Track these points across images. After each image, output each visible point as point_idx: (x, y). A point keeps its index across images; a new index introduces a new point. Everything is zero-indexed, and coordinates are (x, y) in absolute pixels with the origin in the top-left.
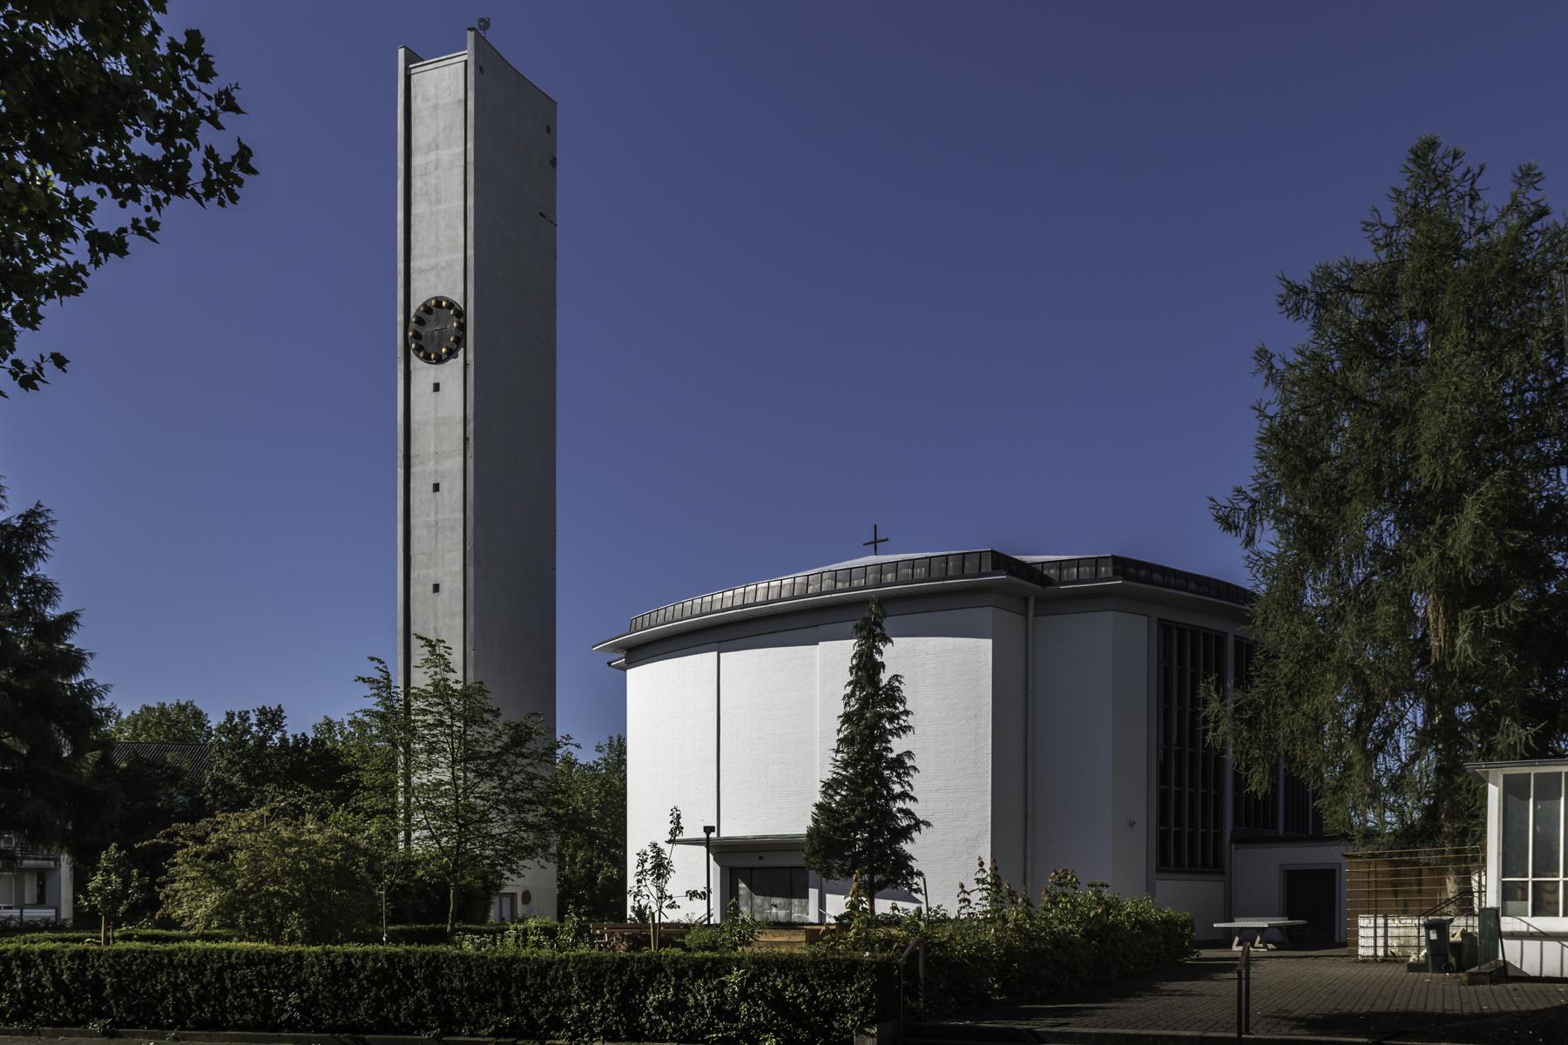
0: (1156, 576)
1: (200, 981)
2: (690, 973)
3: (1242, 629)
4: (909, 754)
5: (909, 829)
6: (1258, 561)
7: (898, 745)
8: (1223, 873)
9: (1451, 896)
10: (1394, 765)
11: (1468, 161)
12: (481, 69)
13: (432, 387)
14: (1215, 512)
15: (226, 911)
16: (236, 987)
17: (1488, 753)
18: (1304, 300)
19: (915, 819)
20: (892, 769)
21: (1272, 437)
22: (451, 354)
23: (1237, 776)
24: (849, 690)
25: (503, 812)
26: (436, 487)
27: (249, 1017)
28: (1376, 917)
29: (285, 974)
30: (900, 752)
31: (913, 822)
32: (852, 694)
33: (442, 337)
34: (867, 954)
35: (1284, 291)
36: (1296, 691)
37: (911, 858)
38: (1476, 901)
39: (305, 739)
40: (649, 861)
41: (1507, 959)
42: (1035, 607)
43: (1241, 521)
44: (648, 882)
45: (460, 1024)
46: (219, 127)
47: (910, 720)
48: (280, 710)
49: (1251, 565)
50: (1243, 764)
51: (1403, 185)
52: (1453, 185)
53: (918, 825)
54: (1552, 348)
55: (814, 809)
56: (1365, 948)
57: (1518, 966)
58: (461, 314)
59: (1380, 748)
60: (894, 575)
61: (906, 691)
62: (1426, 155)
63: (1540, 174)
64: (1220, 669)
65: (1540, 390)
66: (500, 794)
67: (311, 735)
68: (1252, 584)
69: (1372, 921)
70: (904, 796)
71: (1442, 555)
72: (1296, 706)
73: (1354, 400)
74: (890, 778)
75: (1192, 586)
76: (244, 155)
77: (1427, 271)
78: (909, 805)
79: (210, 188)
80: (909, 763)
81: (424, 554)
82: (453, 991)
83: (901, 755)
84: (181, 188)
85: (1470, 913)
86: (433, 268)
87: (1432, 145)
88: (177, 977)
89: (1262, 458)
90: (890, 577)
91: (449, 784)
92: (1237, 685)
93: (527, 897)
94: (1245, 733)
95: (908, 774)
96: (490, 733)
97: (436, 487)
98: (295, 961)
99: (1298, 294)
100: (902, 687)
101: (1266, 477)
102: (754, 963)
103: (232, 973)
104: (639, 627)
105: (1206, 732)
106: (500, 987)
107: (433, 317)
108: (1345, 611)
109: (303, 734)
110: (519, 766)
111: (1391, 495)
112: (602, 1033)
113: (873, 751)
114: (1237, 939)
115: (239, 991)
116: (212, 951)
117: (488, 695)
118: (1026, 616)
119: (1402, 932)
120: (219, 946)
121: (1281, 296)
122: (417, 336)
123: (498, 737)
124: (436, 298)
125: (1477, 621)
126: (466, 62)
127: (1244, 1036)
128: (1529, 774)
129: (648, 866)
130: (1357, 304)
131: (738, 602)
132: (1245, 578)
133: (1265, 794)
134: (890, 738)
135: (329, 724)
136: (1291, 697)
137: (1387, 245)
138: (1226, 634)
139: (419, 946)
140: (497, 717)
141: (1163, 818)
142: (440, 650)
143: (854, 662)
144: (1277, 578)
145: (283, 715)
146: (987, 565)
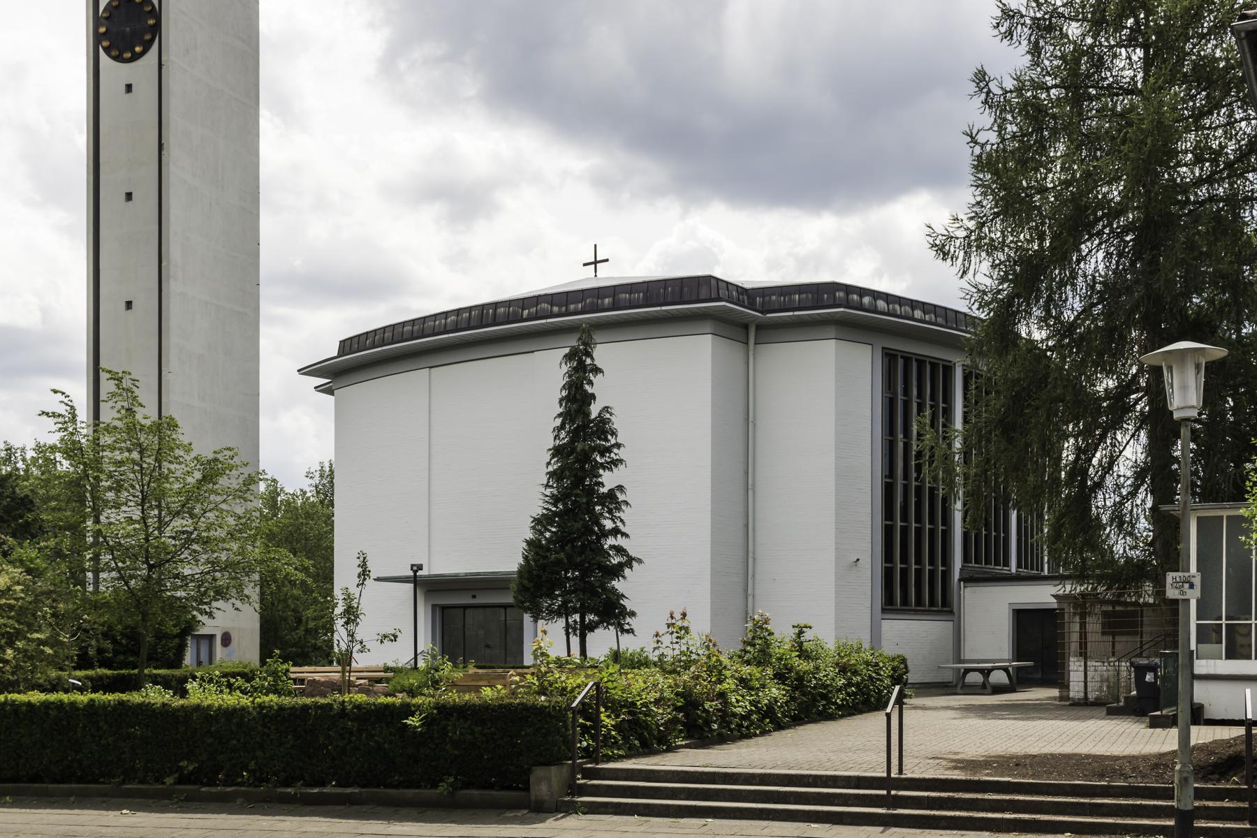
0: (881, 304)
4: (620, 488)
5: (621, 566)
7: (609, 480)
8: (951, 612)
19: (628, 555)
20: (603, 505)
24: (559, 422)
30: (613, 486)
32: (562, 427)
35: (1000, 14)
42: (756, 333)
53: (630, 561)
55: (524, 545)
60: (611, 299)
61: (617, 423)
70: (616, 532)
78: (620, 541)
80: (621, 497)
91: (138, 522)
93: (226, 639)
95: (619, 509)
100: (613, 418)
118: (747, 343)
134: (601, 471)
139: (105, 694)
142: (126, 383)
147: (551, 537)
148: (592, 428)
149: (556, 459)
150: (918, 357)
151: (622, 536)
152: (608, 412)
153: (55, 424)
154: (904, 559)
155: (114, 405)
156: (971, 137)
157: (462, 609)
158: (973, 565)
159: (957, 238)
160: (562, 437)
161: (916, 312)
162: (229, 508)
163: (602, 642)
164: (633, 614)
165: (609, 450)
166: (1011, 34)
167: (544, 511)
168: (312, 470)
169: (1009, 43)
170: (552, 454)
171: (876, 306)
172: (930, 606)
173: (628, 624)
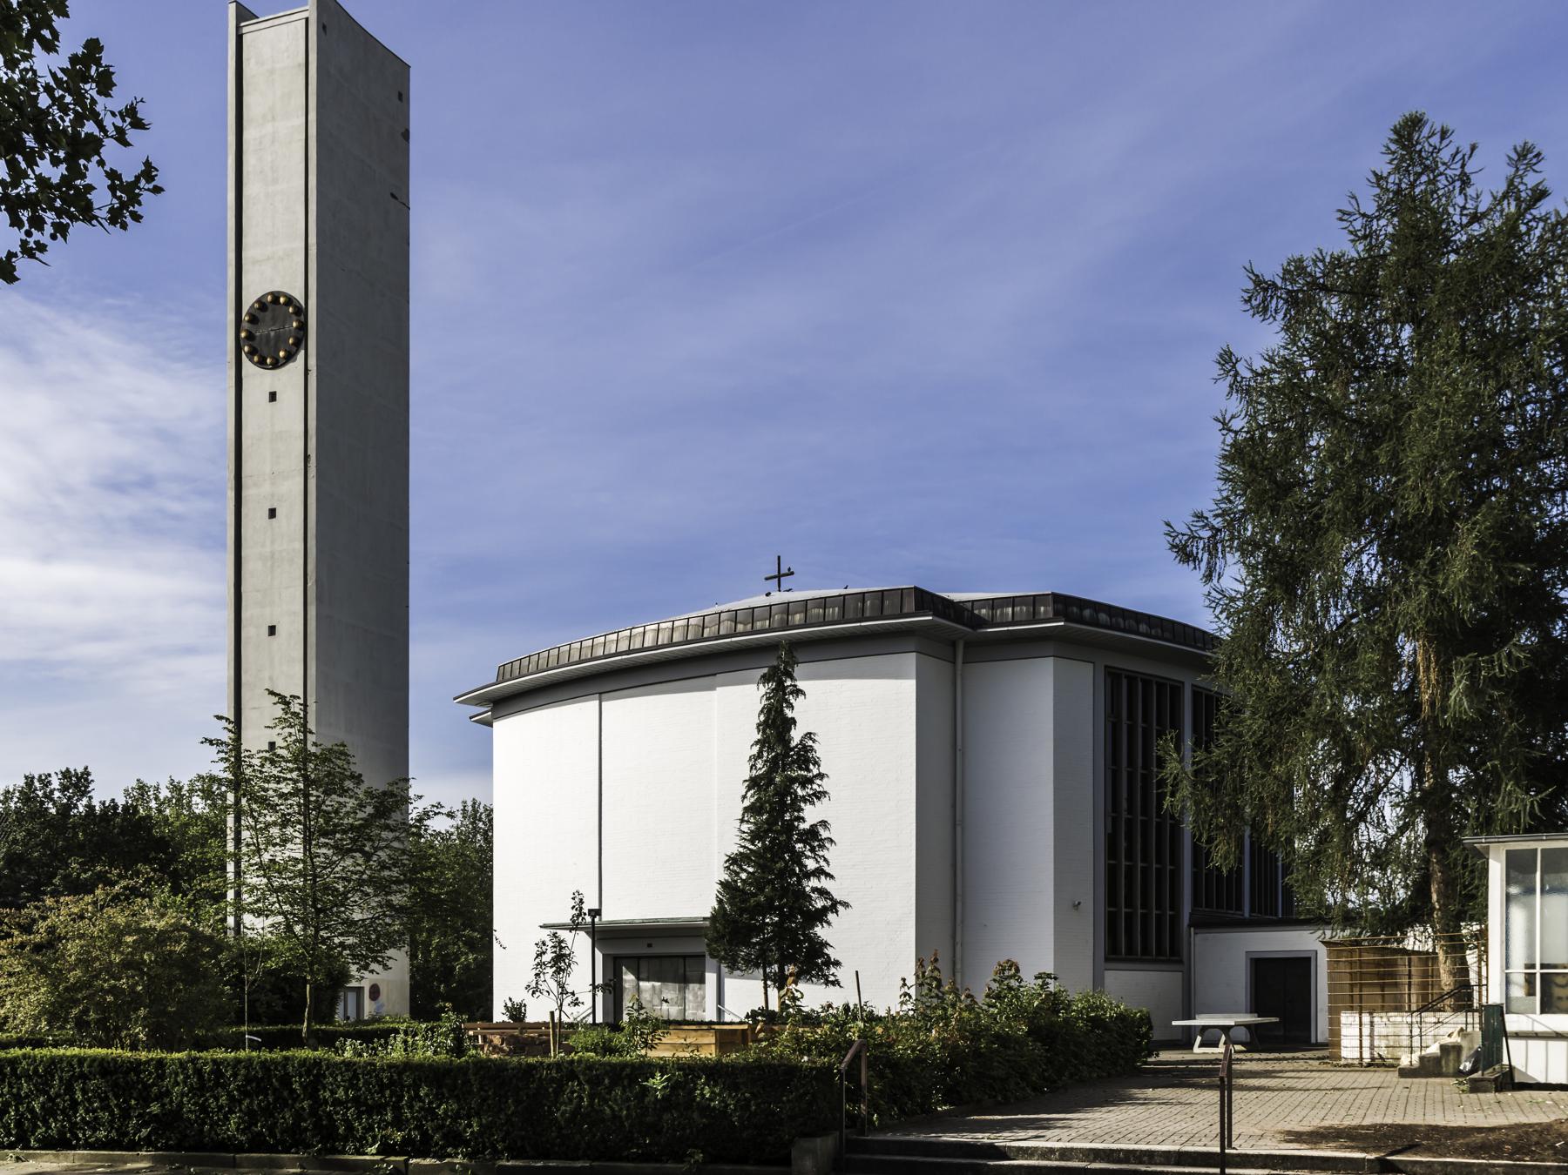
0: (1103, 617)
1: (47, 1093)
2: (607, 1081)
3: (1201, 679)
4: (824, 823)
5: (824, 911)
6: (1225, 603)
7: (811, 815)
8: (1181, 962)
9: (1447, 989)
10: (1377, 836)
11: (1460, 141)
12: (324, 27)
13: (267, 397)
14: (1171, 539)
15: (54, 1014)
16: (89, 1100)
17: (1487, 824)
18: (1272, 297)
20: (805, 842)
21: (1237, 454)
22: (290, 357)
23: (1196, 848)
24: (756, 749)
25: (368, 894)
26: (272, 513)
27: (102, 1134)
28: (1360, 1014)
29: (145, 1084)
30: (815, 822)
31: (830, 903)
32: (759, 755)
33: (279, 340)
34: (806, 1058)
35: (1251, 286)
36: (1267, 752)
37: (826, 944)
38: (1476, 995)
39: (115, 807)
40: (549, 951)
41: (1513, 1064)
42: (964, 653)
43: (1200, 552)
44: (548, 977)
45: (345, 1139)
46: (125, 143)
47: (825, 785)
48: (86, 773)
49: (1214, 605)
50: (1205, 836)
51: (1385, 169)
52: (1442, 168)
53: (834, 907)
54: (1556, 355)
56: (1349, 1050)
57: (1523, 1070)
58: (301, 312)
59: (1361, 816)
60: (803, 615)
61: (820, 750)
62: (1410, 135)
63: (1538, 155)
64: (1176, 724)
65: (1542, 402)
66: (363, 873)
67: (121, 801)
68: (1215, 626)
69: (1357, 1019)
70: (819, 872)
71: (1432, 595)
72: (1267, 767)
73: (1331, 414)
74: (803, 852)
75: (1143, 628)
76: (148, 172)
77: (1414, 266)
78: (824, 883)
79: (115, 217)
80: (824, 834)
81: (258, 591)
82: (337, 1102)
83: (816, 825)
84: (87, 214)
85: (1468, 1008)
86: (268, 259)
87: (1415, 123)
88: (20, 1089)
89: (1226, 480)
90: (798, 618)
92: (1197, 744)
94: (1207, 800)
95: (822, 847)
96: (351, 803)
97: (272, 513)
98: (157, 1069)
99: (1266, 290)
100: (816, 746)
101: (1230, 502)
102: (679, 1069)
103: (84, 1083)
104: (508, 676)
105: (1161, 797)
106: (391, 1097)
107: (268, 314)
108: (1322, 659)
109: (113, 801)
110: (384, 840)
111: (1374, 524)
112: (506, 1149)
113: (783, 821)
114: (1199, 1039)
115: (91, 1104)
116: (61, 1059)
117: (352, 760)
118: (954, 663)
119: (1391, 1030)
120: (69, 1053)
121: (1246, 291)
122: (250, 337)
123: (361, 806)
124: (272, 293)
125: (1474, 670)
126: (307, 20)
127: (1227, 1151)
128: (1536, 849)
129: (547, 957)
130: (1333, 305)
131: (623, 647)
132: (1208, 620)
133: (1230, 871)
134: (802, 805)
135: (142, 788)
136: (1260, 758)
137: (1365, 237)
138: (1183, 683)
140: (358, 784)
141: (1112, 898)
143: (762, 718)
144: (1243, 620)
145: (90, 778)
146: (910, 605)
147: (748, 878)
148: (792, 756)
149: (752, 791)
150: (1143, 677)
151: (826, 877)
152: (811, 739)
153: (219, 752)
154: (1129, 903)
155: (280, 731)
156: (1224, 423)
157: (681, 960)
158: (1204, 909)
159: (1201, 538)
160: (759, 766)
161: (1141, 626)
162: (402, 847)
163: (812, 996)
164: (837, 964)
165: (811, 781)
166: (1265, 310)
167: (741, 850)
168: (454, 810)
169: (1262, 318)
170: (748, 786)
171: (1098, 619)
172: (1143, 954)
173: (833, 975)
